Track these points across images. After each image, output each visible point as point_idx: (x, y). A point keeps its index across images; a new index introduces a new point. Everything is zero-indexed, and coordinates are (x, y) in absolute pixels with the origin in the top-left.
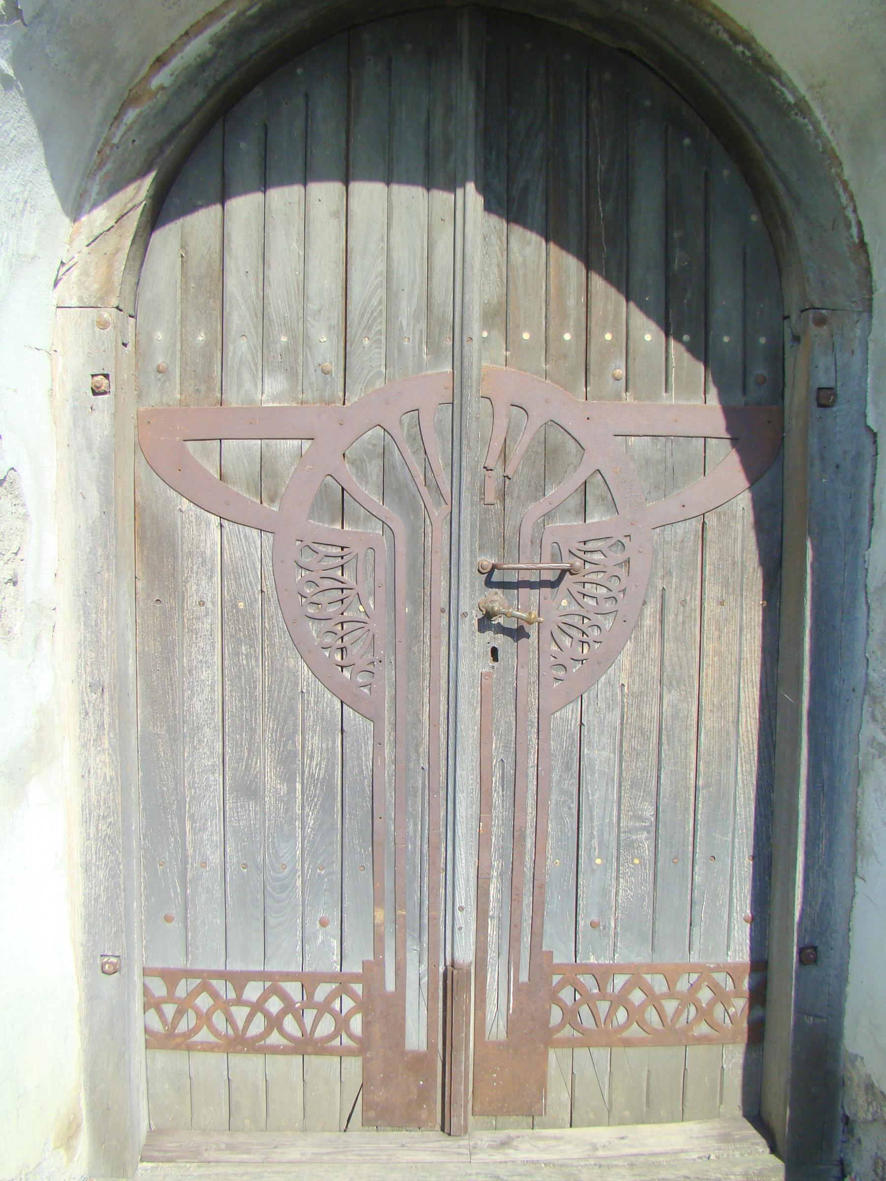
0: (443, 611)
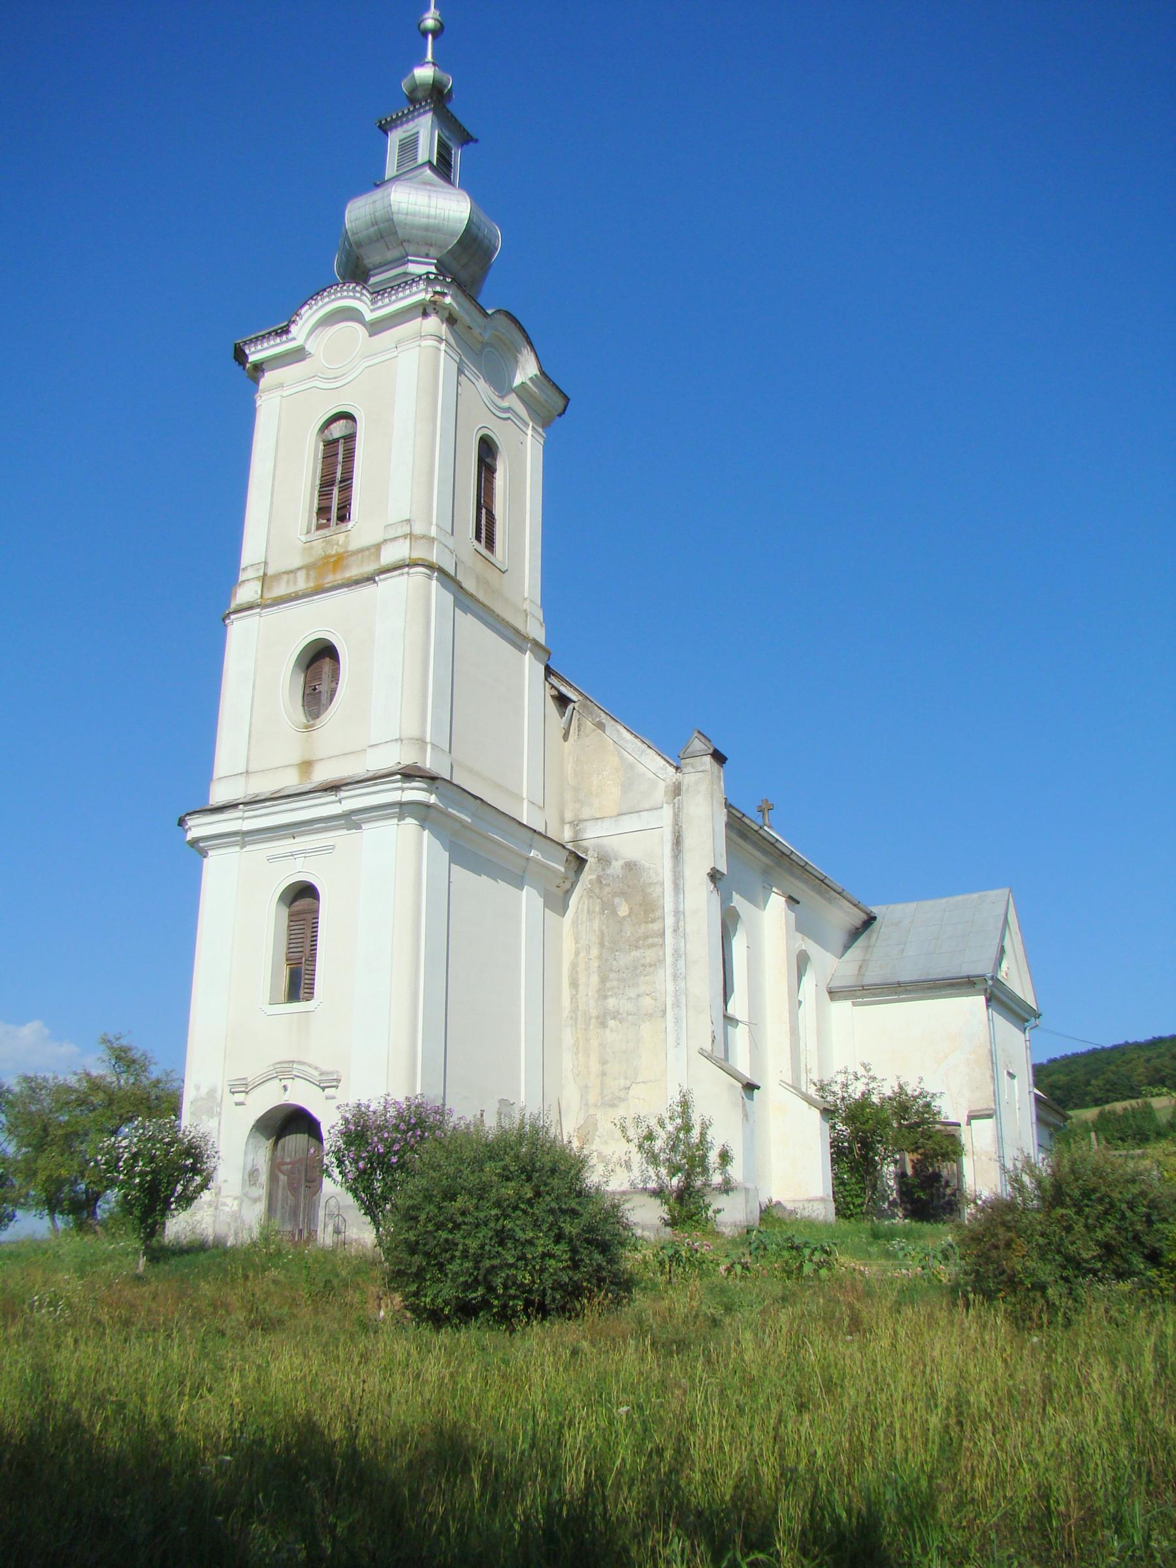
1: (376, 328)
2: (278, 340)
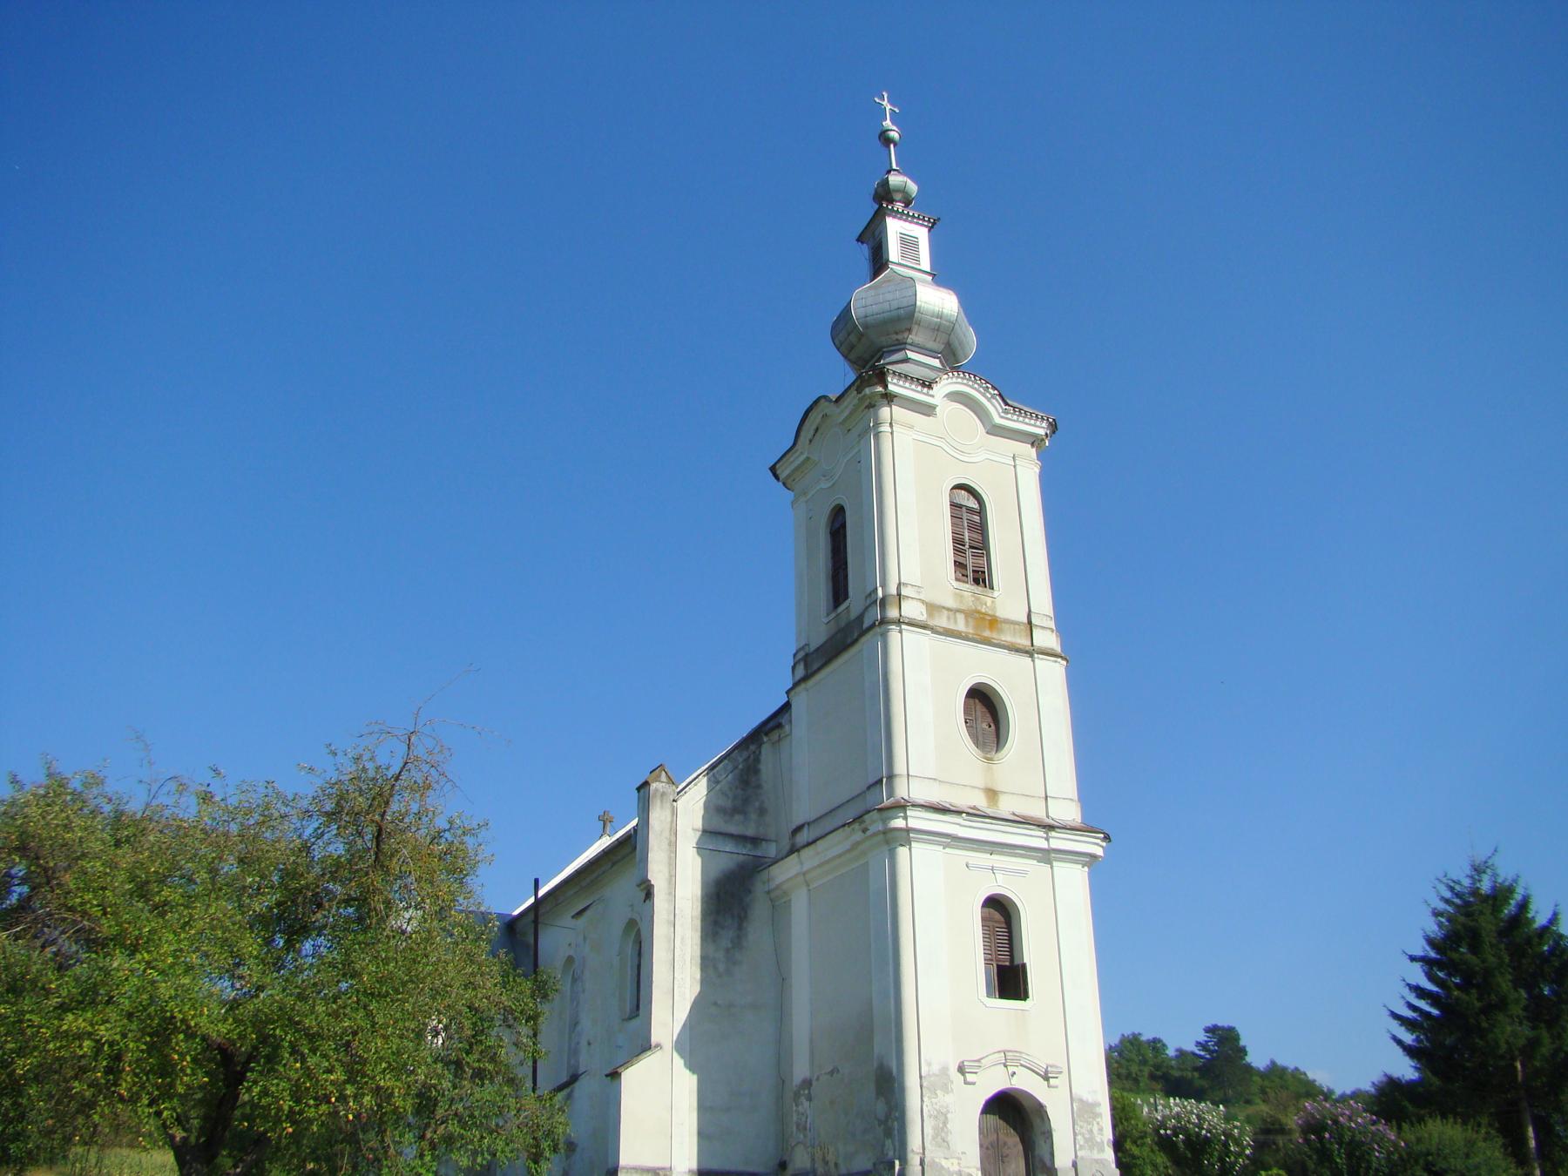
0: (992, 794)
1: (995, 430)
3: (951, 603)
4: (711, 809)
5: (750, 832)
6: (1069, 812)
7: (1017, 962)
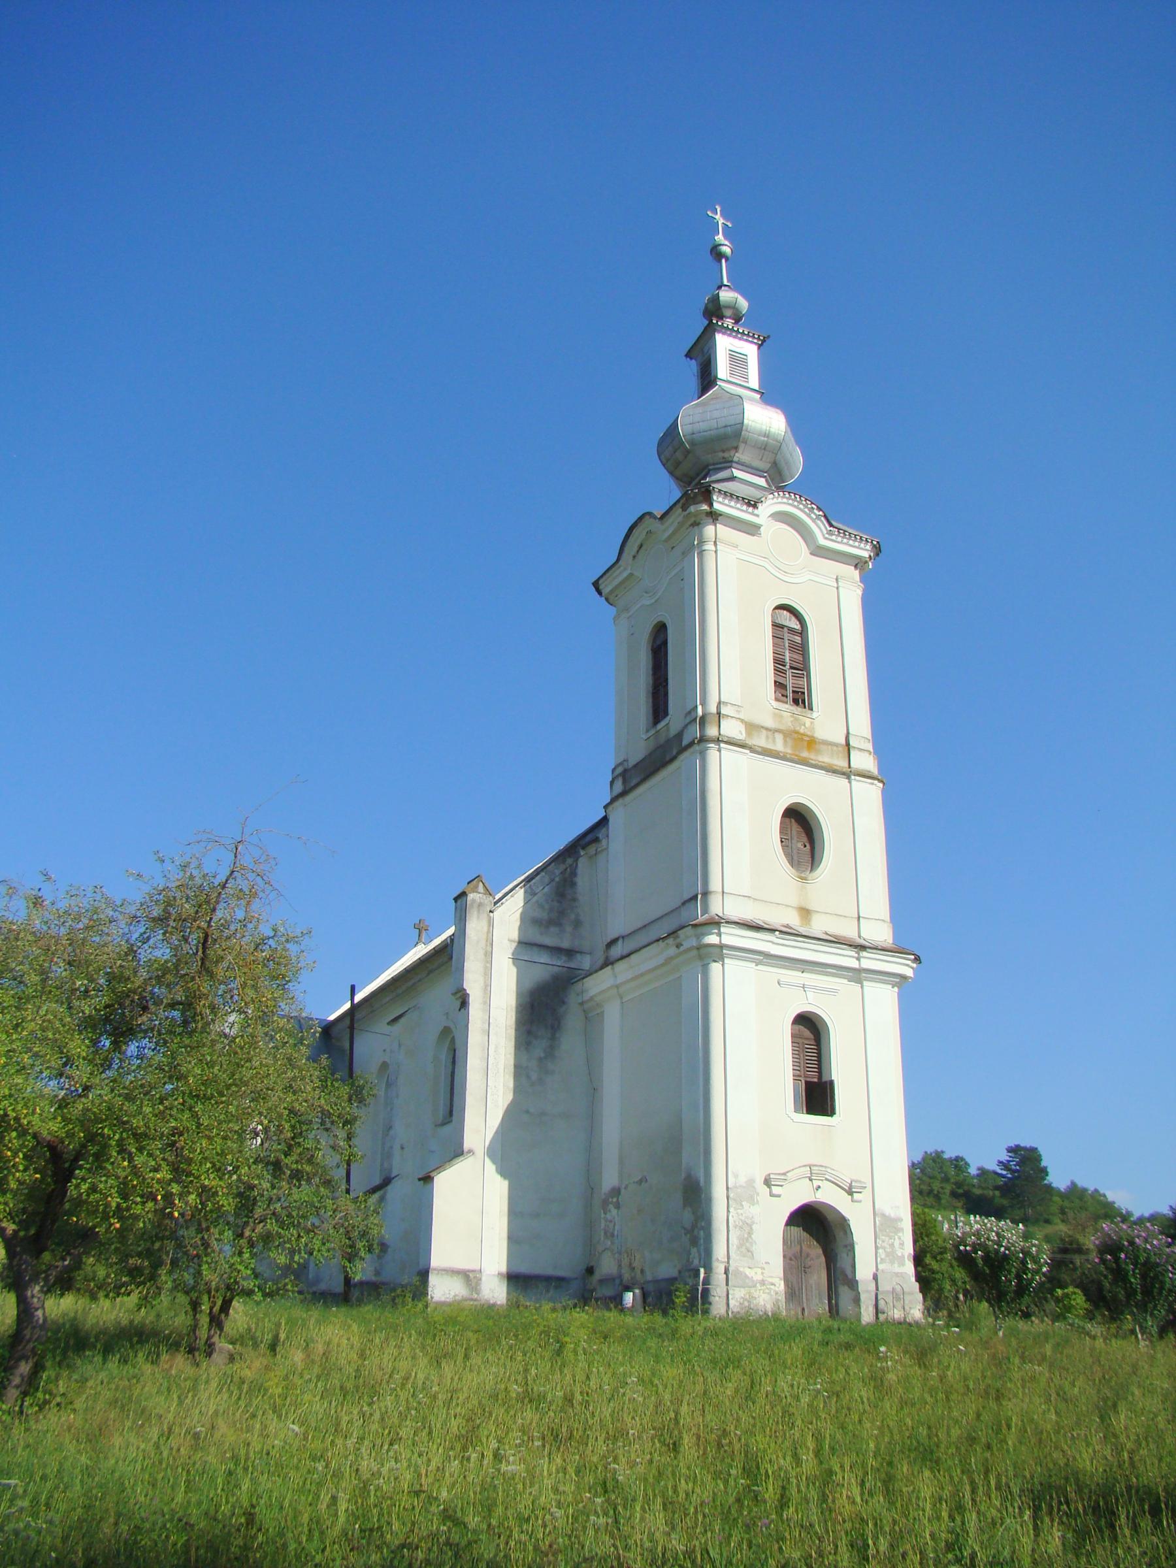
0: (805, 913)
1: (819, 552)
2: (745, 508)
3: (769, 723)
4: (528, 920)
5: (565, 944)
6: (880, 932)
7: (825, 1079)
